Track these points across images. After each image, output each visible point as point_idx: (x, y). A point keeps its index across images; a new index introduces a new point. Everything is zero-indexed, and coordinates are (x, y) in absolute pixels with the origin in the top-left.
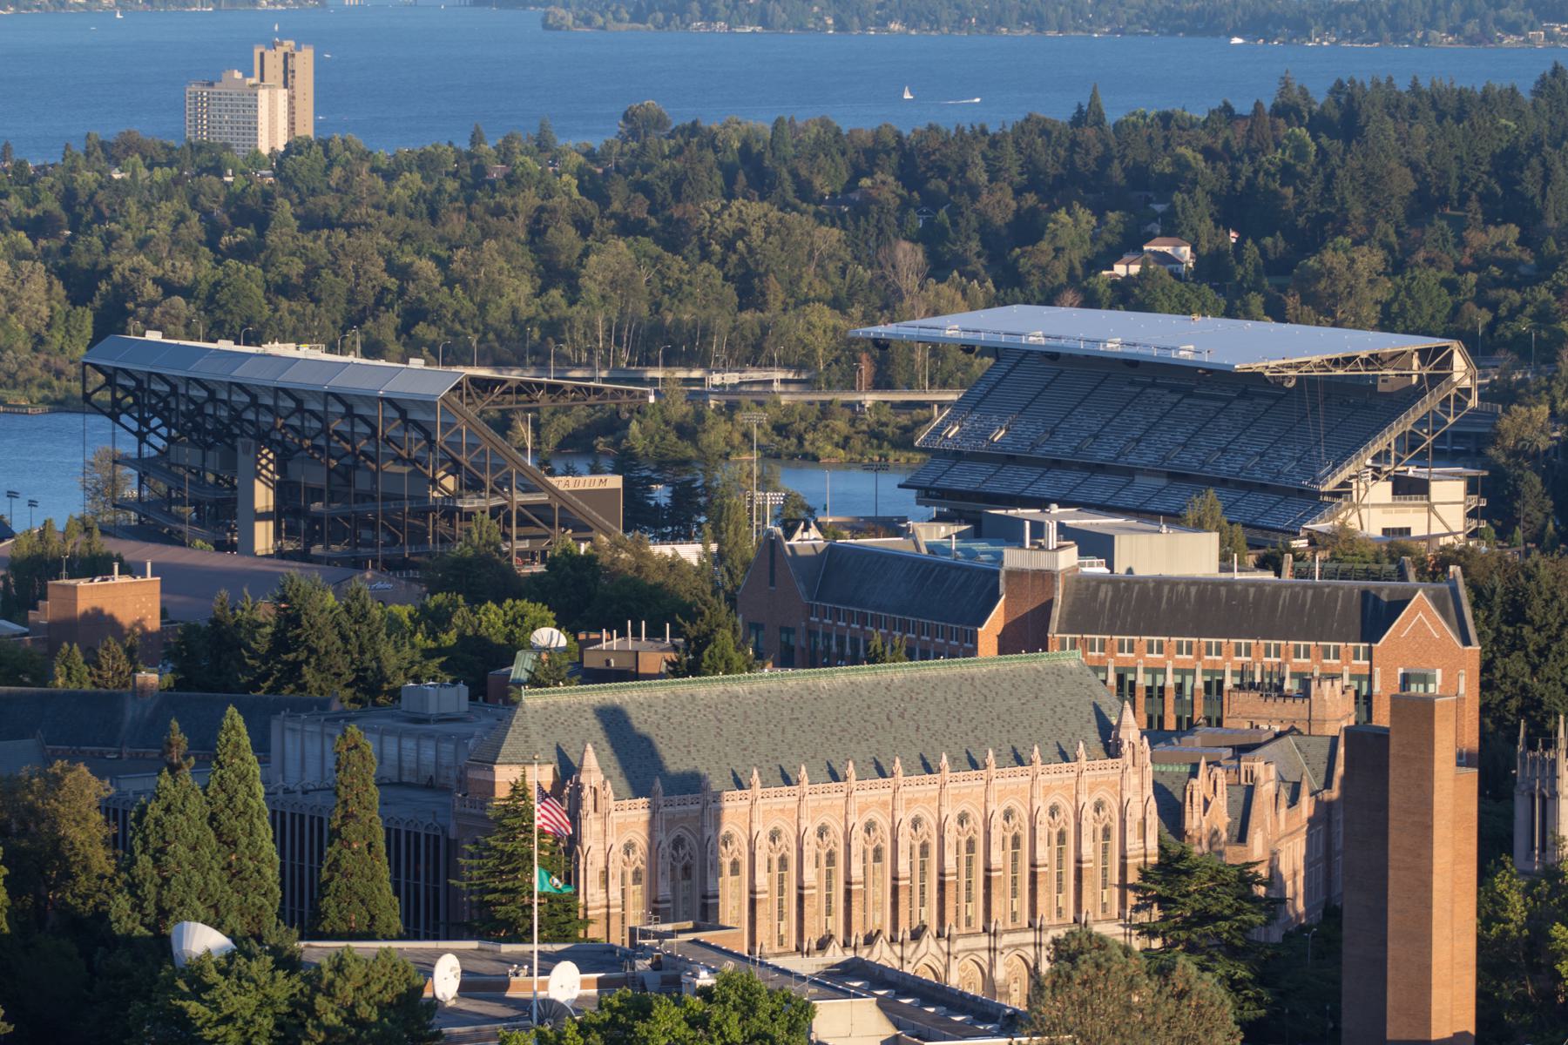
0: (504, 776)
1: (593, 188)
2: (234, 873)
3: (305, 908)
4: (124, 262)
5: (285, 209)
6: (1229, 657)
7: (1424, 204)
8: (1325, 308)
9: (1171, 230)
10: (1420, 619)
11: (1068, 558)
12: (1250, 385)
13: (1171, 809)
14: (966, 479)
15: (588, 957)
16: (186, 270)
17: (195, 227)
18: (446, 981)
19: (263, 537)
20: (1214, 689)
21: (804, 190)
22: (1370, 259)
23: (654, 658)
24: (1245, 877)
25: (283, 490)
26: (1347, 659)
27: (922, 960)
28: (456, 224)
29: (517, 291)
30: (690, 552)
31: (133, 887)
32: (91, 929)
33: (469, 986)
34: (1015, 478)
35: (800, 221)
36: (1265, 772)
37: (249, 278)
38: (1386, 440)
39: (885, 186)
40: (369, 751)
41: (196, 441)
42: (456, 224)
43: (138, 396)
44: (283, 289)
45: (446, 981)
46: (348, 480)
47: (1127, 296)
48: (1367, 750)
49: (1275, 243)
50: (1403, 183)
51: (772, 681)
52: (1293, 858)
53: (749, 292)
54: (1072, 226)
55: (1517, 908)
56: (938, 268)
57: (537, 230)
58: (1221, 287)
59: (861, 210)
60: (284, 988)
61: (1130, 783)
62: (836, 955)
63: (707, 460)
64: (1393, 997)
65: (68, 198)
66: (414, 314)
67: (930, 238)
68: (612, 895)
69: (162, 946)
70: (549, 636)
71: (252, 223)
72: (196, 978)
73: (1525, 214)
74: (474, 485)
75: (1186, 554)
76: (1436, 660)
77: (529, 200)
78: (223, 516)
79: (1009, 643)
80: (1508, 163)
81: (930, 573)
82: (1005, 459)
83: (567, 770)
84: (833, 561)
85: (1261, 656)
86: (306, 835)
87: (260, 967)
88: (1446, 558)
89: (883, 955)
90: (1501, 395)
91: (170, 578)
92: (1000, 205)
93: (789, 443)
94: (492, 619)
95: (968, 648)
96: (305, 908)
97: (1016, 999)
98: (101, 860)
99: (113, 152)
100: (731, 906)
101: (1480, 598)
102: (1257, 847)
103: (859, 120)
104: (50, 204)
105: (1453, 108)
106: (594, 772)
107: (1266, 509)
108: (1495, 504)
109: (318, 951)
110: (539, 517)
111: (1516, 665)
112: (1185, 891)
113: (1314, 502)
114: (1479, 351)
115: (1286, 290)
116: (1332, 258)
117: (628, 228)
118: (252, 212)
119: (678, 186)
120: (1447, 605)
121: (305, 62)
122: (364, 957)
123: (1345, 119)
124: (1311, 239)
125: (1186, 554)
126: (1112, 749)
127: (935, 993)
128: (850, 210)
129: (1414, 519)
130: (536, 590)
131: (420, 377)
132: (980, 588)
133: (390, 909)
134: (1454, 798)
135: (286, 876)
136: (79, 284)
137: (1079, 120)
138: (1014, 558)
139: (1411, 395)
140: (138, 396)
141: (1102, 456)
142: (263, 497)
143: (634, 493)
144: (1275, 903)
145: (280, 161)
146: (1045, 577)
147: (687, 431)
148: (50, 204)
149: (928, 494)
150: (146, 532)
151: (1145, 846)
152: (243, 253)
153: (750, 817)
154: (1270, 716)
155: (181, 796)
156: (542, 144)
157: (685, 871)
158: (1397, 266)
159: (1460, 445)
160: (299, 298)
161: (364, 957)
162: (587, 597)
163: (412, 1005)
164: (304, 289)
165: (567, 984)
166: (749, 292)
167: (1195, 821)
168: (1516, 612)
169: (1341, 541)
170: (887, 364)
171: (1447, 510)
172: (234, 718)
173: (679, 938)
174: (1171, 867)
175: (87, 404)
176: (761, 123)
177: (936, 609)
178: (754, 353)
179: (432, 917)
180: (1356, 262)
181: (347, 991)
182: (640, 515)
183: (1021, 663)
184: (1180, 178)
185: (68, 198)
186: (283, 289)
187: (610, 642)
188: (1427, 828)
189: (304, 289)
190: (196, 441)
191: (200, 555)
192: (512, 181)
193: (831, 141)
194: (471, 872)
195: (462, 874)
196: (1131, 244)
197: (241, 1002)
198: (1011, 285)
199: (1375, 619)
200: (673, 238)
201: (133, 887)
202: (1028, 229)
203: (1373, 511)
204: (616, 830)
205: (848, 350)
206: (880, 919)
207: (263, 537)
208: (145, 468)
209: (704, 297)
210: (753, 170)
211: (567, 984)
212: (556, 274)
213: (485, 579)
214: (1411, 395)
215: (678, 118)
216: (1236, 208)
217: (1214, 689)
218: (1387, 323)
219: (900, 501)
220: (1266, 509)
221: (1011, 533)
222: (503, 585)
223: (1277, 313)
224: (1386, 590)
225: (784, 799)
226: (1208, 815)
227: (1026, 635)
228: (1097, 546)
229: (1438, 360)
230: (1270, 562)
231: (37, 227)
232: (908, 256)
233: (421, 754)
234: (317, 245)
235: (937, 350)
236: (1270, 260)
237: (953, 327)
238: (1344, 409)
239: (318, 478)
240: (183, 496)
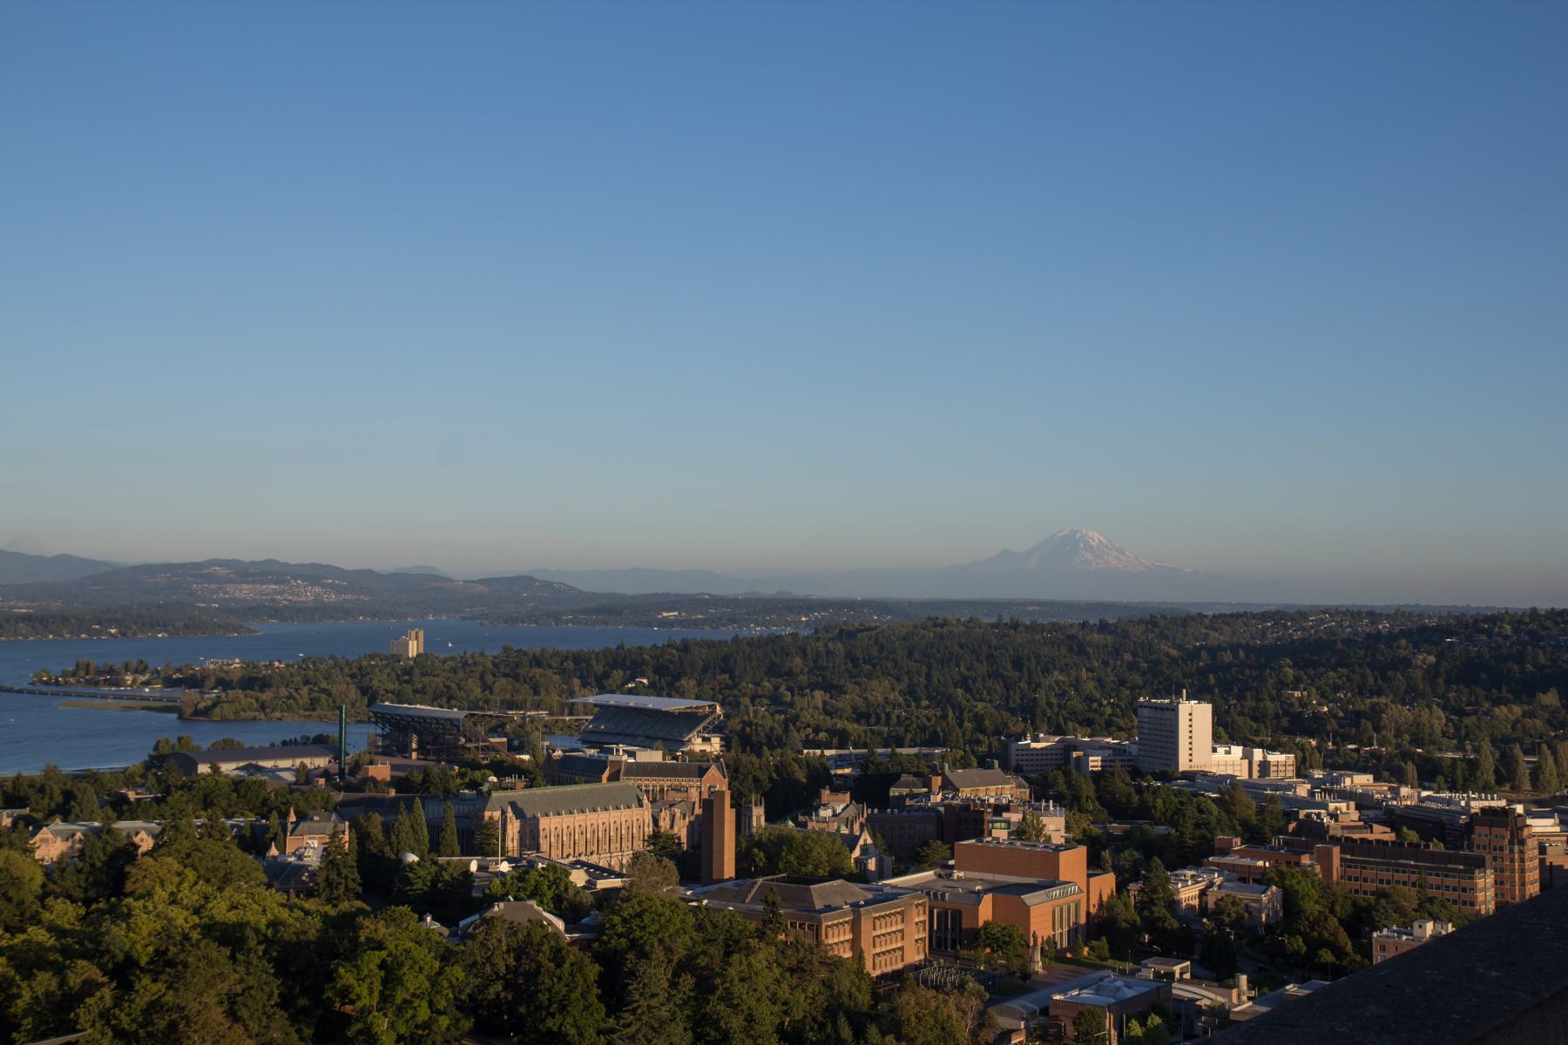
0: (487, 814)
1: (495, 665)
2: (417, 841)
3: (436, 846)
4: (375, 683)
5: (417, 671)
6: (666, 782)
7: (705, 670)
8: (682, 695)
9: (643, 676)
10: (713, 772)
11: (625, 757)
12: (667, 714)
13: (656, 821)
14: (594, 738)
15: (510, 860)
16: (391, 687)
17: (393, 676)
18: (474, 867)
19: (414, 755)
20: (662, 790)
21: (550, 666)
22: (692, 683)
23: (520, 784)
24: (673, 837)
25: (420, 743)
26: (695, 782)
27: (593, 859)
28: (461, 674)
29: (477, 691)
30: (526, 757)
31: (391, 845)
32: (379, 858)
33: (480, 868)
34: (608, 738)
35: (549, 672)
36: (678, 811)
37: (407, 688)
38: (700, 728)
39: (570, 665)
40: (452, 810)
41: (397, 733)
42: (461, 674)
43: (382, 718)
44: (416, 691)
45: (474, 867)
46: (436, 738)
47: (631, 692)
48: (708, 805)
49: (668, 679)
50: (700, 664)
51: (550, 790)
52: (683, 834)
53: (536, 693)
54: (618, 675)
55: (744, 844)
56: (584, 685)
57: (482, 677)
58: (654, 690)
59: (564, 670)
60: (434, 869)
61: (645, 814)
62: (571, 859)
63: (528, 734)
64: (714, 867)
65: (360, 669)
66: (450, 698)
67: (581, 677)
68: (512, 844)
69: (400, 861)
70: (494, 779)
71: (409, 676)
72: (411, 866)
73: (730, 672)
74: (470, 741)
75: (655, 756)
76: (716, 780)
77: (480, 668)
78: (404, 749)
79: (609, 779)
80: (726, 659)
81: (590, 761)
82: (603, 733)
83: (504, 813)
84: (564, 759)
85: (675, 781)
86: (436, 830)
87: (428, 864)
88: (717, 758)
89: (583, 858)
90: (727, 716)
91: (394, 767)
92: (599, 669)
93: (549, 730)
94: (477, 775)
95: (600, 780)
96: (436, 846)
97: (617, 869)
98: (381, 837)
99: (371, 657)
100: (544, 846)
101: (728, 766)
102: (676, 830)
103: (563, 648)
104: (355, 670)
105: (711, 645)
106: (510, 814)
107: (672, 743)
108: (727, 744)
109: (442, 860)
110: (486, 749)
111: (736, 784)
112: (659, 842)
113: (683, 744)
114: (722, 706)
115: (673, 690)
116: (684, 682)
117: (505, 675)
118: (408, 671)
119: (518, 665)
120: (720, 769)
121: (421, 634)
122: (450, 860)
123: (685, 648)
124: (678, 677)
125: (655, 756)
126: (641, 805)
127: (597, 867)
128: (562, 671)
129: (707, 748)
130: (487, 767)
131: (455, 713)
132: (602, 765)
133: (457, 848)
134: (729, 815)
135: (431, 841)
136: (364, 691)
137: (618, 648)
138: (611, 758)
139: (706, 716)
140: (382, 718)
141: (629, 731)
142: (414, 746)
143: (510, 741)
144: (680, 844)
145: (414, 659)
146: (620, 762)
147: (521, 726)
148: (355, 670)
149: (584, 742)
150: (383, 754)
151: (649, 830)
152: (406, 682)
153: (548, 824)
154: (678, 797)
155: (403, 821)
156: (482, 654)
157: (530, 836)
158: (699, 685)
159: (718, 729)
160: (421, 694)
161: (450, 860)
162: (501, 769)
163: (467, 874)
164: (423, 691)
165: (505, 867)
166: (536, 693)
167: (661, 823)
168: (736, 770)
169: (691, 753)
170: (572, 710)
171: (715, 745)
172: (418, 800)
173: (533, 855)
174: (656, 837)
175: (369, 722)
176: (538, 650)
177: (592, 771)
178: (538, 707)
179: (469, 849)
180: (688, 683)
181: (450, 870)
182: (511, 748)
183: (615, 784)
184: (644, 662)
185: (360, 669)
186: (416, 691)
187: (508, 780)
188: (723, 824)
189: (423, 691)
190: (397, 733)
191: (399, 760)
192: (475, 664)
193: (556, 654)
194: (478, 838)
195: (477, 839)
196: (632, 679)
197: (422, 873)
198: (603, 690)
199: (702, 772)
200: (516, 678)
201: (391, 845)
202: (606, 675)
203: (697, 745)
204: (514, 827)
205: (562, 706)
206: (582, 849)
207: (414, 755)
208: (384, 737)
209: (525, 692)
210: (537, 661)
211: (505, 867)
212: (486, 687)
213: (476, 766)
214: (706, 716)
215: (1210, 613)
216: (660, 670)
217: (662, 790)
218: (697, 698)
219: (579, 745)
220: (672, 743)
221: (610, 751)
222: (476, 766)
223: (669, 696)
224: (704, 765)
225: (617, 813)
226: (664, 824)
227: (614, 777)
228: (632, 754)
229: (713, 707)
230: (675, 758)
231: (352, 676)
232: (576, 682)
233: (466, 809)
234: (426, 680)
235: (585, 705)
236: (667, 681)
237: (591, 700)
238: (690, 720)
239: (430, 738)
240: (393, 746)
